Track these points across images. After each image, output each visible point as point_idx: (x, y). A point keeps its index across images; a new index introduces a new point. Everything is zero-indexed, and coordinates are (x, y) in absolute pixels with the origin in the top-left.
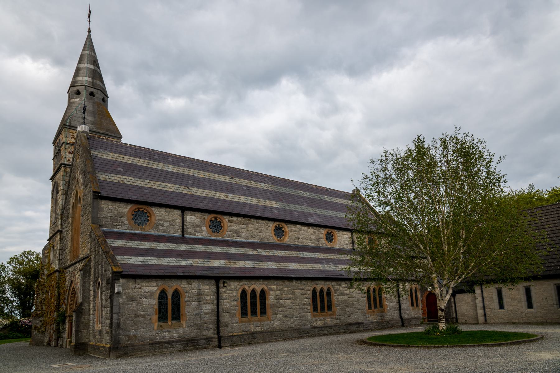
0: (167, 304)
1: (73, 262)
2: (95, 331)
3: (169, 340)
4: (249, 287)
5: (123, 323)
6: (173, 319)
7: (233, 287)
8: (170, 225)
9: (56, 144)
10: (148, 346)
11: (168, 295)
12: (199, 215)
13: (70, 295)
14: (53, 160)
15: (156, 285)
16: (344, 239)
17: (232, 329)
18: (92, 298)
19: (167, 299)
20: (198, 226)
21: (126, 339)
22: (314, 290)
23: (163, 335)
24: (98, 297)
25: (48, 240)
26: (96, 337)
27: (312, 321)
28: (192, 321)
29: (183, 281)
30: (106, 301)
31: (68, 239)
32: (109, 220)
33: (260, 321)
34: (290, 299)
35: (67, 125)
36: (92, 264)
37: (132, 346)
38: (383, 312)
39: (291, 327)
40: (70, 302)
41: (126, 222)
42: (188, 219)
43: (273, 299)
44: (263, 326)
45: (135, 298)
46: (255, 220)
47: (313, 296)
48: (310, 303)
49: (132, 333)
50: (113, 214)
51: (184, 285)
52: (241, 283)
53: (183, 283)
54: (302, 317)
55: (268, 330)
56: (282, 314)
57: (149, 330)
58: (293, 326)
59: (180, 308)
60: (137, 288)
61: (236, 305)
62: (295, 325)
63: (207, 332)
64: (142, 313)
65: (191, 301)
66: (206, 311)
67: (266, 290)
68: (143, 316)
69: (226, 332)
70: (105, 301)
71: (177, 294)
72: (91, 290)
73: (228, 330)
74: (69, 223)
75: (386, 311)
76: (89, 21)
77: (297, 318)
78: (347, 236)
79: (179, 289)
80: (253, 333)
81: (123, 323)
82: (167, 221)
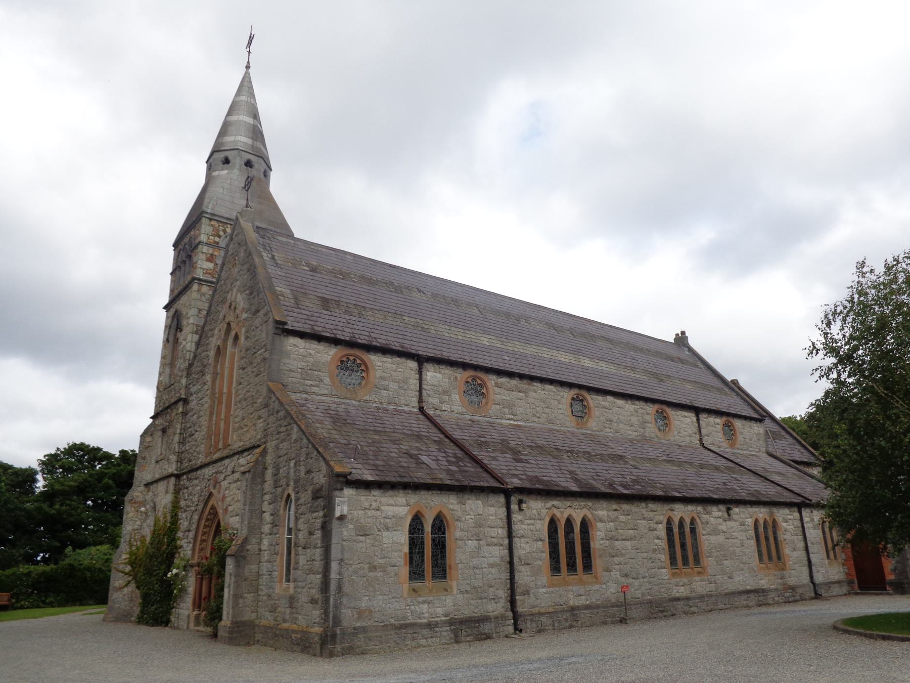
0: (423, 543)
1: (217, 456)
2: (276, 598)
3: (428, 621)
4: (562, 513)
5: (349, 581)
6: (434, 576)
7: (535, 512)
8: (400, 387)
9: (180, 247)
10: (392, 633)
11: (425, 525)
12: (447, 371)
13: (203, 521)
14: (171, 274)
15: (405, 502)
16: (685, 426)
17: (537, 599)
18: (266, 528)
19: (423, 534)
20: (445, 392)
21: (353, 616)
22: (669, 522)
23: (418, 609)
24: (285, 526)
25: (151, 418)
26: (279, 609)
27: (670, 586)
28: (468, 582)
29: (451, 497)
30: (311, 533)
31: (202, 414)
32: (299, 376)
33: (581, 582)
34: (631, 539)
35: (207, 213)
36: (269, 459)
37: (364, 629)
38: (783, 569)
39: (636, 597)
40: (202, 536)
41: (327, 380)
42: (429, 378)
43: (602, 539)
44: (589, 595)
45: (370, 528)
46: (539, 385)
47: (667, 535)
48: (663, 549)
49: (364, 604)
50: (306, 364)
51: (452, 504)
52: (549, 504)
53: (451, 501)
54: (653, 577)
55: (598, 602)
56: (620, 570)
57: (394, 598)
58: (640, 596)
59: (445, 552)
60: (374, 509)
61: (542, 549)
62: (643, 594)
63: (494, 604)
64: (382, 561)
65: (464, 538)
66: (491, 560)
67: (589, 520)
68: (383, 569)
69: (526, 604)
70: (306, 534)
71: (440, 525)
72: (264, 512)
73: (530, 601)
74: (205, 384)
75: (788, 568)
76: (249, 52)
77: (645, 580)
78: (690, 420)
79: (445, 512)
80: (573, 609)
81: (349, 581)
82: (394, 381)
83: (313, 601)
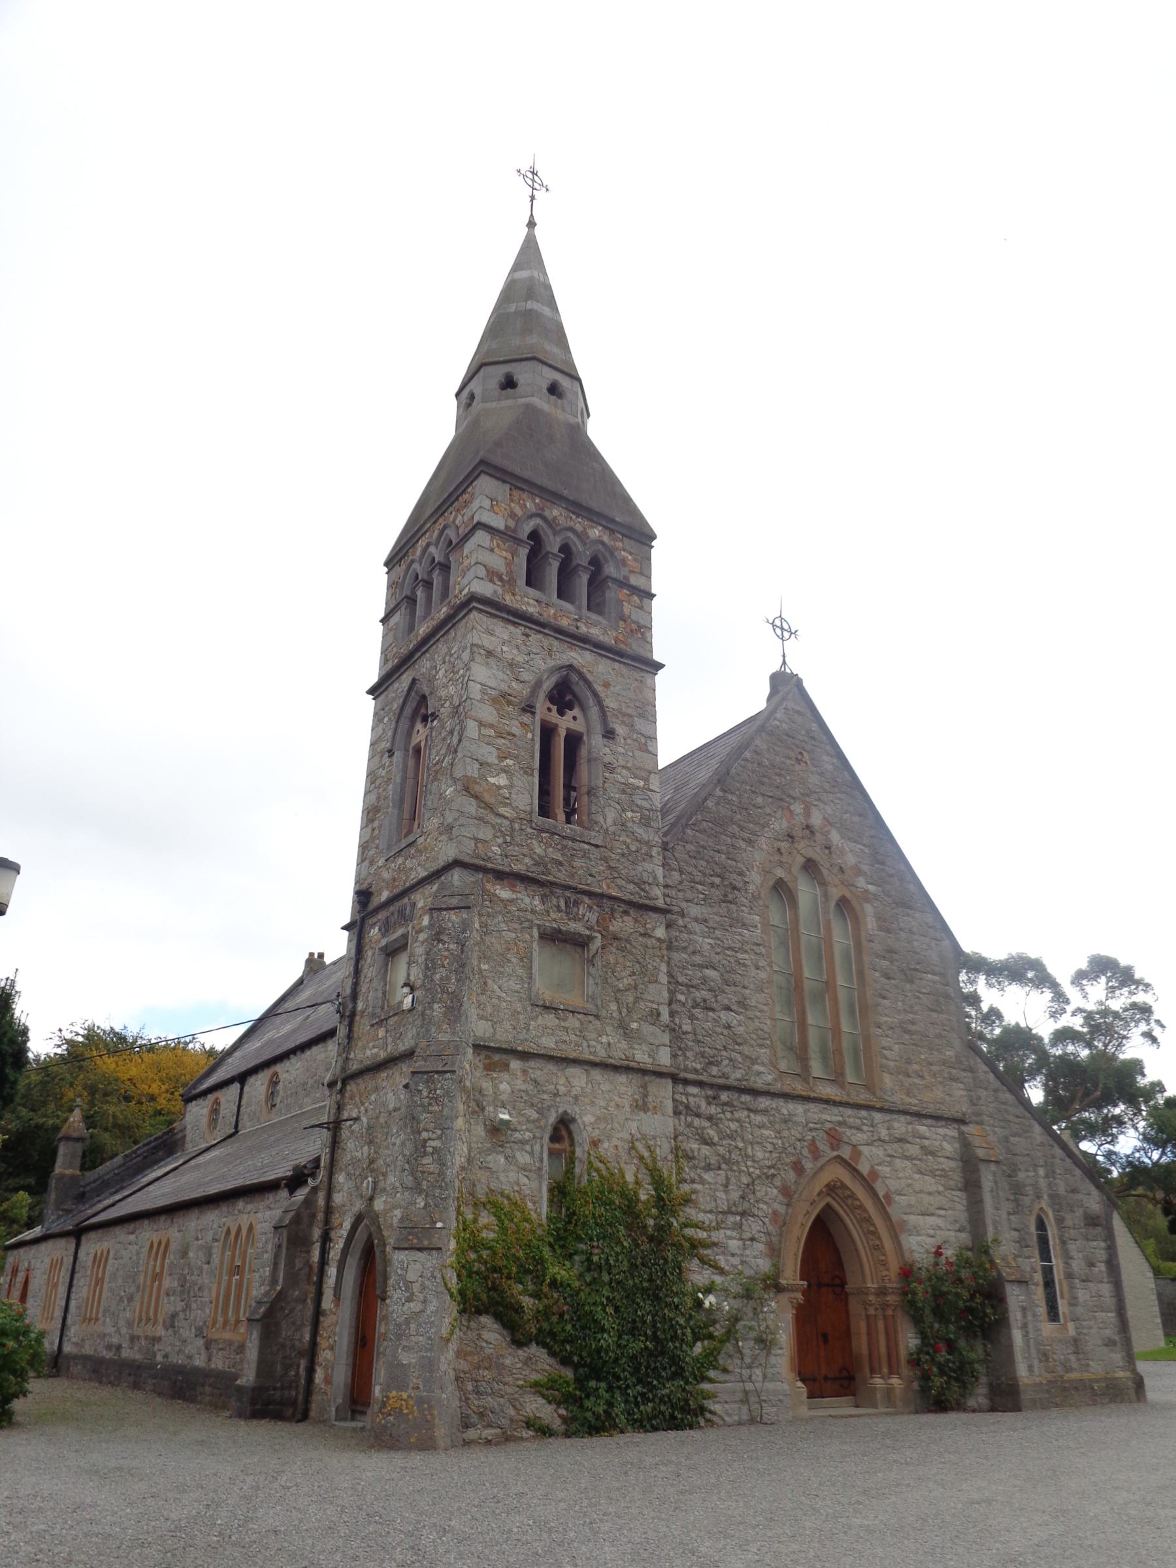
83: (1110, 1343)
